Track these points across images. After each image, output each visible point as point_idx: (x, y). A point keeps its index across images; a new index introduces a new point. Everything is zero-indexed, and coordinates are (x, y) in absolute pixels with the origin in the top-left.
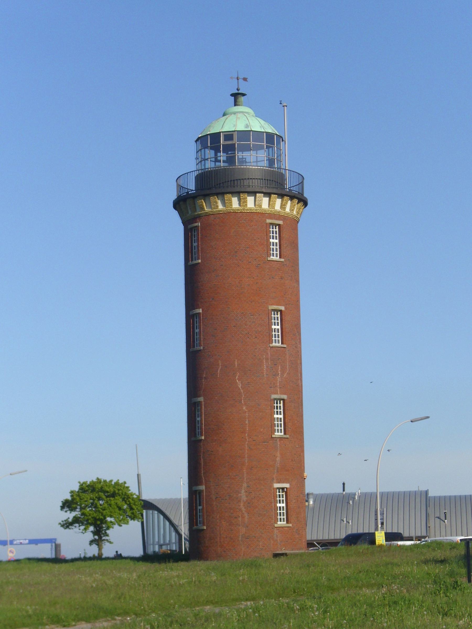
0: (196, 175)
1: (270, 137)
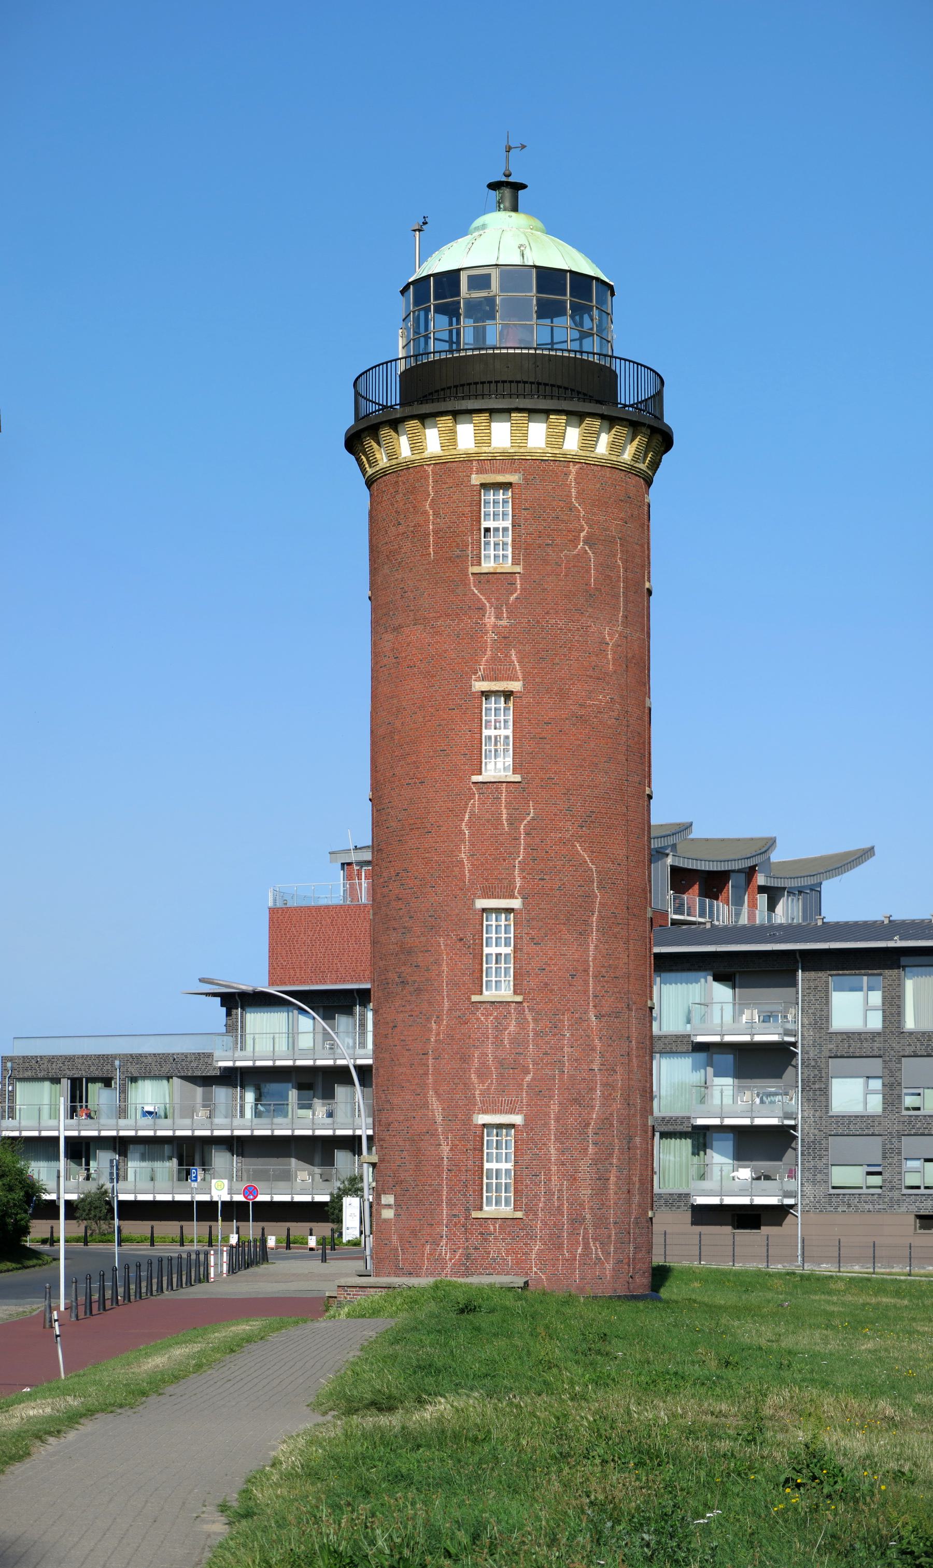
0: (403, 369)
1: (582, 282)
